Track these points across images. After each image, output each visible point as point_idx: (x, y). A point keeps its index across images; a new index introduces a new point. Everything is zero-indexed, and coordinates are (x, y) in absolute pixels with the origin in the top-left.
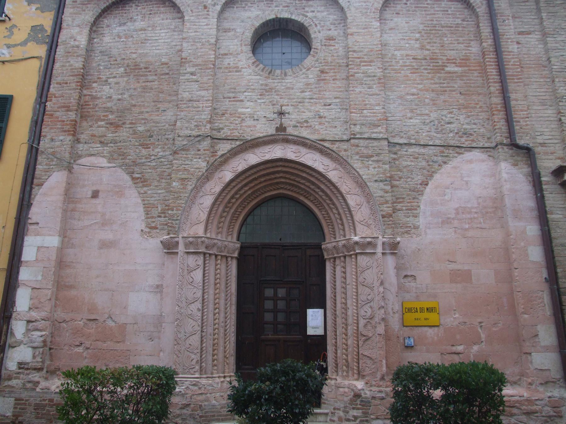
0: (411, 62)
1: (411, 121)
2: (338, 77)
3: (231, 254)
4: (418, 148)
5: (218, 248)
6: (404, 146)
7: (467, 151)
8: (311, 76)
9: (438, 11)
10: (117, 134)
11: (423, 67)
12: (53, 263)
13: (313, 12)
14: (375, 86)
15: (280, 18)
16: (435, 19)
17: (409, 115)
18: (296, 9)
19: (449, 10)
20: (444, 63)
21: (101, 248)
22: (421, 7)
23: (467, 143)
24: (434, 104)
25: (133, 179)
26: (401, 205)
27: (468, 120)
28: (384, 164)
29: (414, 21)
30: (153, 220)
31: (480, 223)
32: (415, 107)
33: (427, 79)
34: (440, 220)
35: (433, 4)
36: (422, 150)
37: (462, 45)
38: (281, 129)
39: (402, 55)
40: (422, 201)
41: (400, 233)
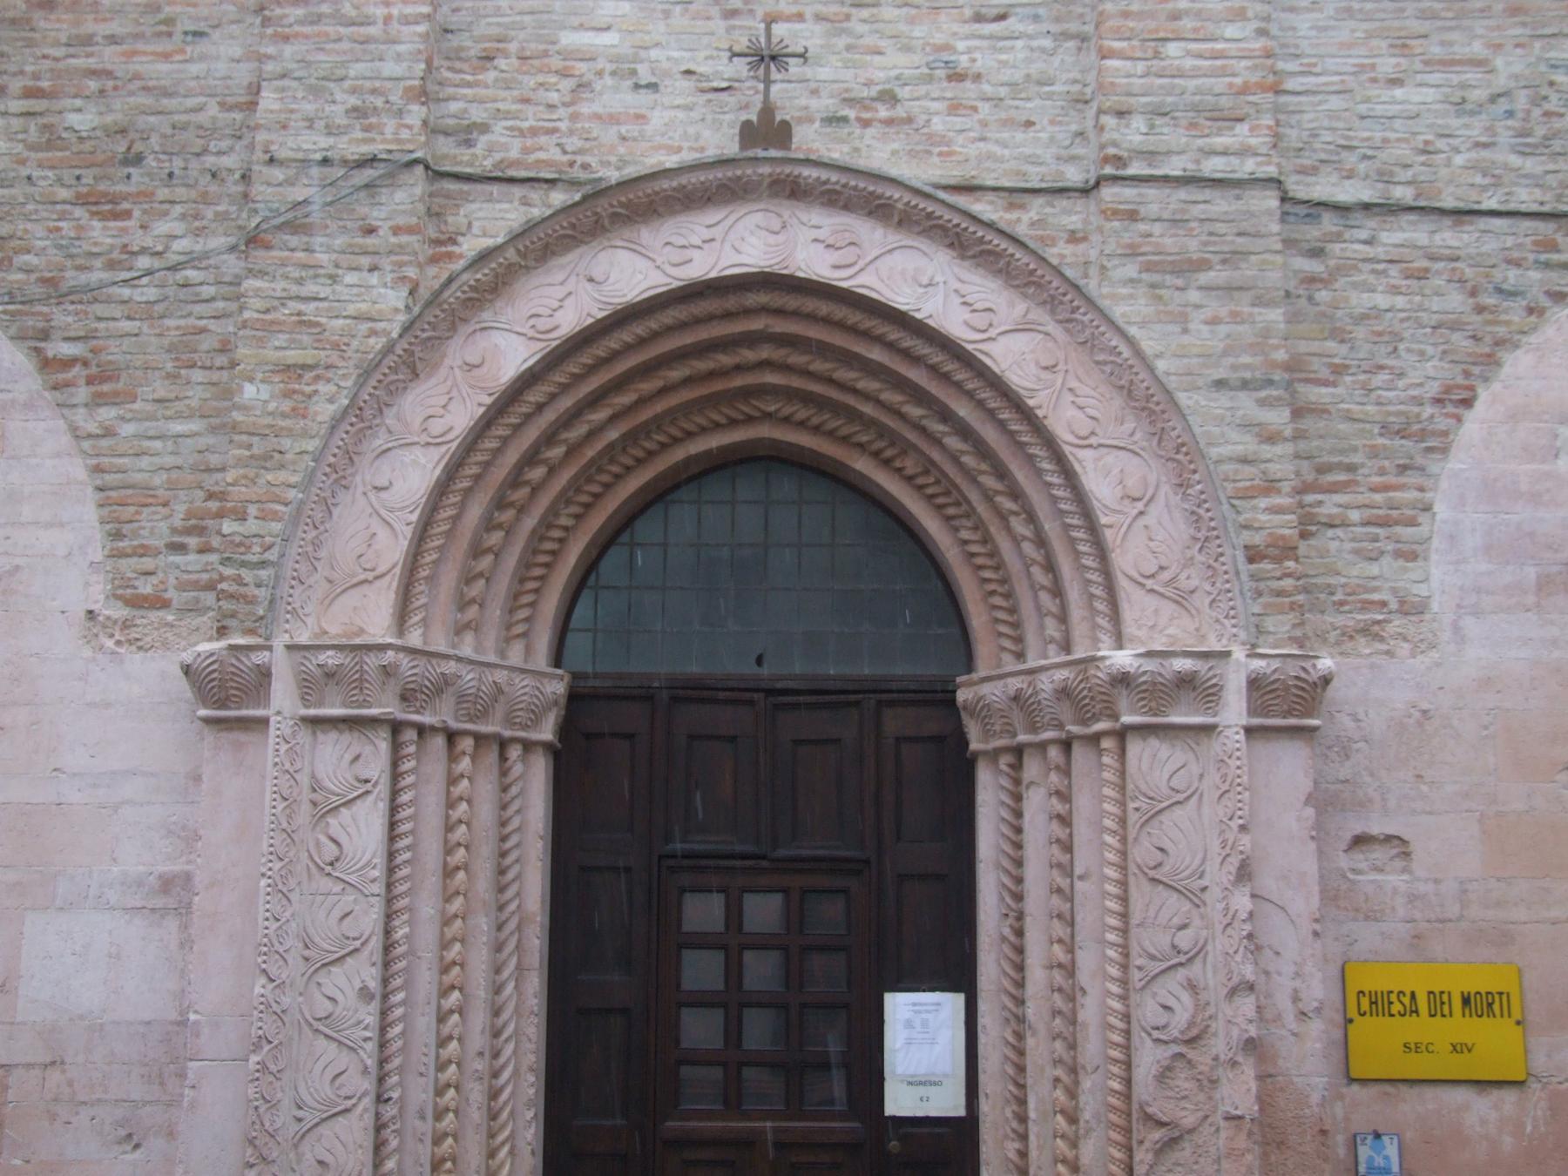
1: (1398, 93)
3: (525, 727)
6: (1357, 217)
17: (1388, 65)
25: (47, 364)
28: (1259, 302)
30: (148, 563)
32: (1417, 26)
34: (1531, 572)
36: (1448, 237)
38: (767, 131)
40: (1444, 484)
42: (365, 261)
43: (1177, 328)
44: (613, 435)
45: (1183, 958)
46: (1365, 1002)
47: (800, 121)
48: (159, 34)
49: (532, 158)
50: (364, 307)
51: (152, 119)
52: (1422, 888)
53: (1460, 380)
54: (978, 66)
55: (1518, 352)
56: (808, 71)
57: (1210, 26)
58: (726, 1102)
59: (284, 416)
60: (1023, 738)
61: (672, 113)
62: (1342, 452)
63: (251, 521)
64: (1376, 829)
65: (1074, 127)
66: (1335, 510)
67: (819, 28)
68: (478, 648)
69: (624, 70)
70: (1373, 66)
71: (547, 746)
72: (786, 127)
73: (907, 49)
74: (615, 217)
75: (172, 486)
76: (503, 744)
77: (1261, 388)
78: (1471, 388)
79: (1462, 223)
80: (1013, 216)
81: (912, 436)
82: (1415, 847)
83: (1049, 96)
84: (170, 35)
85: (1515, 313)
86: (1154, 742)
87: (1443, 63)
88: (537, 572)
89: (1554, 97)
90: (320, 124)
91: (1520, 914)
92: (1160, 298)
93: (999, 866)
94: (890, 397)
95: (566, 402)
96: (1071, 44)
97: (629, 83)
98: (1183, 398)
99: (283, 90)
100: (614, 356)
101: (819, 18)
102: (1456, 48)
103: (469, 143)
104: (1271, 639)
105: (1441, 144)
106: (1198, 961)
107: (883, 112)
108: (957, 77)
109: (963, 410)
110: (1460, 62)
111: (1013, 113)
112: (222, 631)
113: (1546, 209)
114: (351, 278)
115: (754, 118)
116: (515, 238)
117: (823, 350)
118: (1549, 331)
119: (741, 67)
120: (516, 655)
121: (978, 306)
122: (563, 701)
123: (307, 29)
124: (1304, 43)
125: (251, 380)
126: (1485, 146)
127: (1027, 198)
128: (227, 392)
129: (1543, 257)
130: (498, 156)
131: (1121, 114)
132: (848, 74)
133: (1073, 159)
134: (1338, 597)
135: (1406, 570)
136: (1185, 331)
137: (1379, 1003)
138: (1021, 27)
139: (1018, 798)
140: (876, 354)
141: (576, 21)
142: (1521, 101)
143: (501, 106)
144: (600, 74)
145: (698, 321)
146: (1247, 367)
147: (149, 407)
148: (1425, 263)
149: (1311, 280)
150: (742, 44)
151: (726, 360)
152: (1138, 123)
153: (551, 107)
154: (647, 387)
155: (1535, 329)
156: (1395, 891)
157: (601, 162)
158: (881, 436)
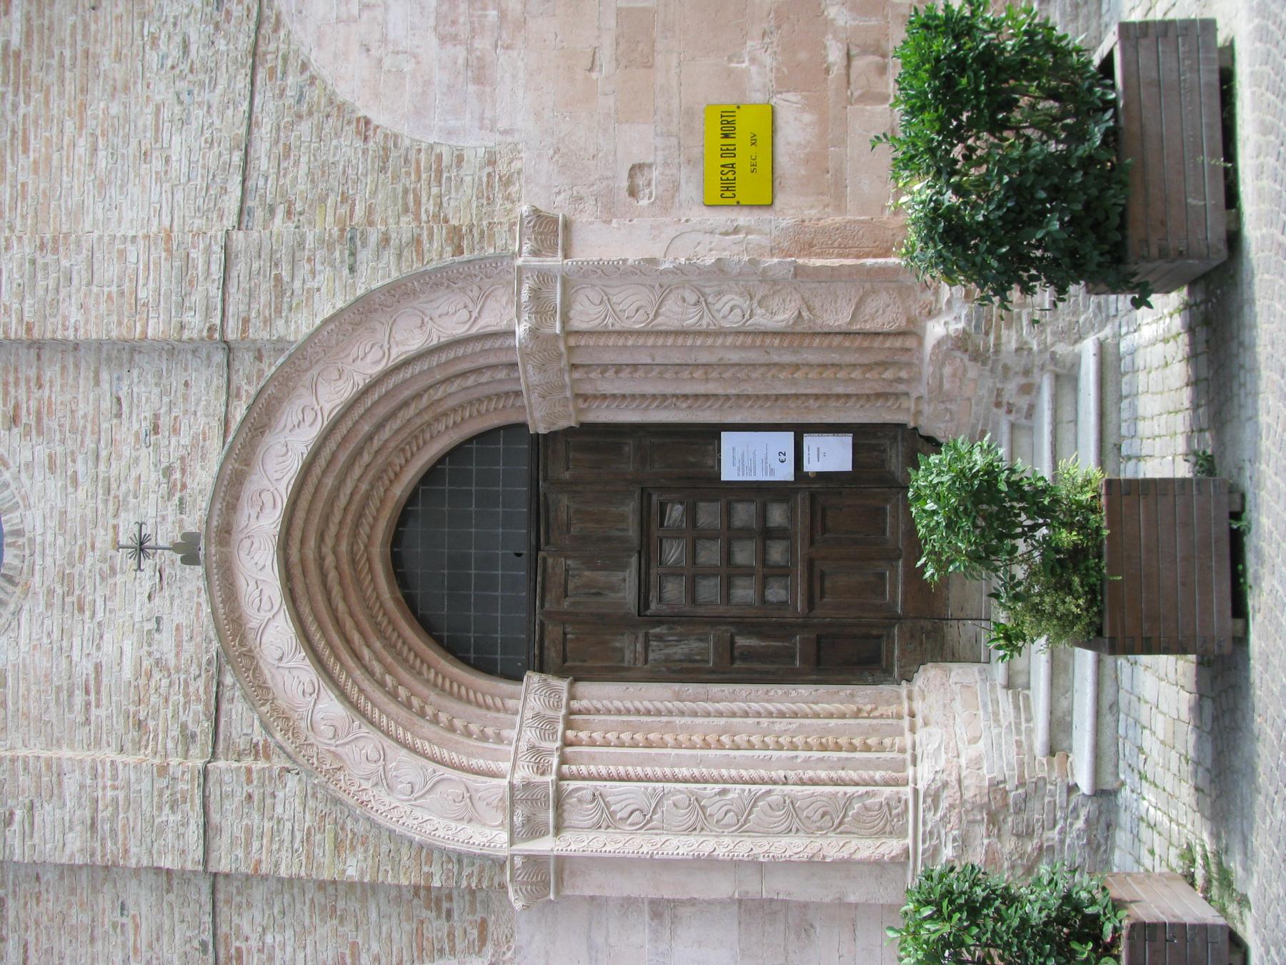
17: (157, 165)
24: (126, 89)
32: (134, 143)
34: (472, 88)
36: (264, 131)
38: (188, 551)
42: (269, 801)
44: (378, 645)
45: (702, 299)
47: (181, 527)
48: (123, 932)
49: (203, 697)
50: (297, 801)
51: (177, 936)
52: (660, 159)
54: (149, 415)
55: (338, 91)
56: (151, 522)
57: (129, 271)
58: (787, 576)
59: (366, 851)
60: (568, 394)
61: (175, 607)
62: (396, 197)
63: (432, 870)
64: (625, 184)
65: (189, 356)
66: (431, 201)
67: (123, 515)
68: (513, 726)
69: (148, 638)
70: (157, 173)
71: (571, 685)
72: (184, 536)
73: (137, 460)
74: (242, 644)
76: (571, 712)
77: (354, 244)
78: (358, 120)
79: (257, 122)
80: (244, 394)
81: (380, 459)
82: (637, 161)
83: (169, 371)
84: (123, 925)
85: (313, 94)
86: (572, 314)
87: (157, 131)
88: (463, 690)
90: (181, 830)
91: (675, 103)
92: (298, 305)
93: (646, 409)
94: (357, 471)
95: (358, 673)
96: (137, 357)
97: (157, 636)
98: (359, 292)
99: (159, 852)
100: (329, 644)
101: (116, 516)
102: (148, 123)
103: (194, 736)
104: (510, 242)
105: (207, 134)
107: (177, 475)
108: (156, 430)
109: (366, 428)
111: (179, 394)
112: (503, 886)
113: (249, 72)
114: (279, 809)
115: (179, 556)
116: (253, 707)
117: (326, 518)
119: (146, 564)
121: (300, 417)
122: (543, 676)
123: (121, 837)
124: (141, 215)
125: (344, 871)
126: (209, 107)
127: (233, 386)
128: (351, 885)
129: (279, 75)
130: (202, 717)
131: (182, 327)
132: (152, 496)
133: (209, 357)
135: (468, 161)
136: (318, 290)
137: (728, 186)
138: (125, 389)
139: (604, 397)
140: (329, 482)
141: (116, 668)
142: (182, 85)
143: (170, 716)
144: (150, 654)
146: (342, 253)
147: (361, 934)
148: (281, 145)
149: (289, 213)
150: (132, 563)
151: (332, 575)
152: (188, 317)
153: (170, 685)
154: (349, 624)
155: (324, 81)
156: (662, 174)
157: (207, 652)
158: (380, 478)
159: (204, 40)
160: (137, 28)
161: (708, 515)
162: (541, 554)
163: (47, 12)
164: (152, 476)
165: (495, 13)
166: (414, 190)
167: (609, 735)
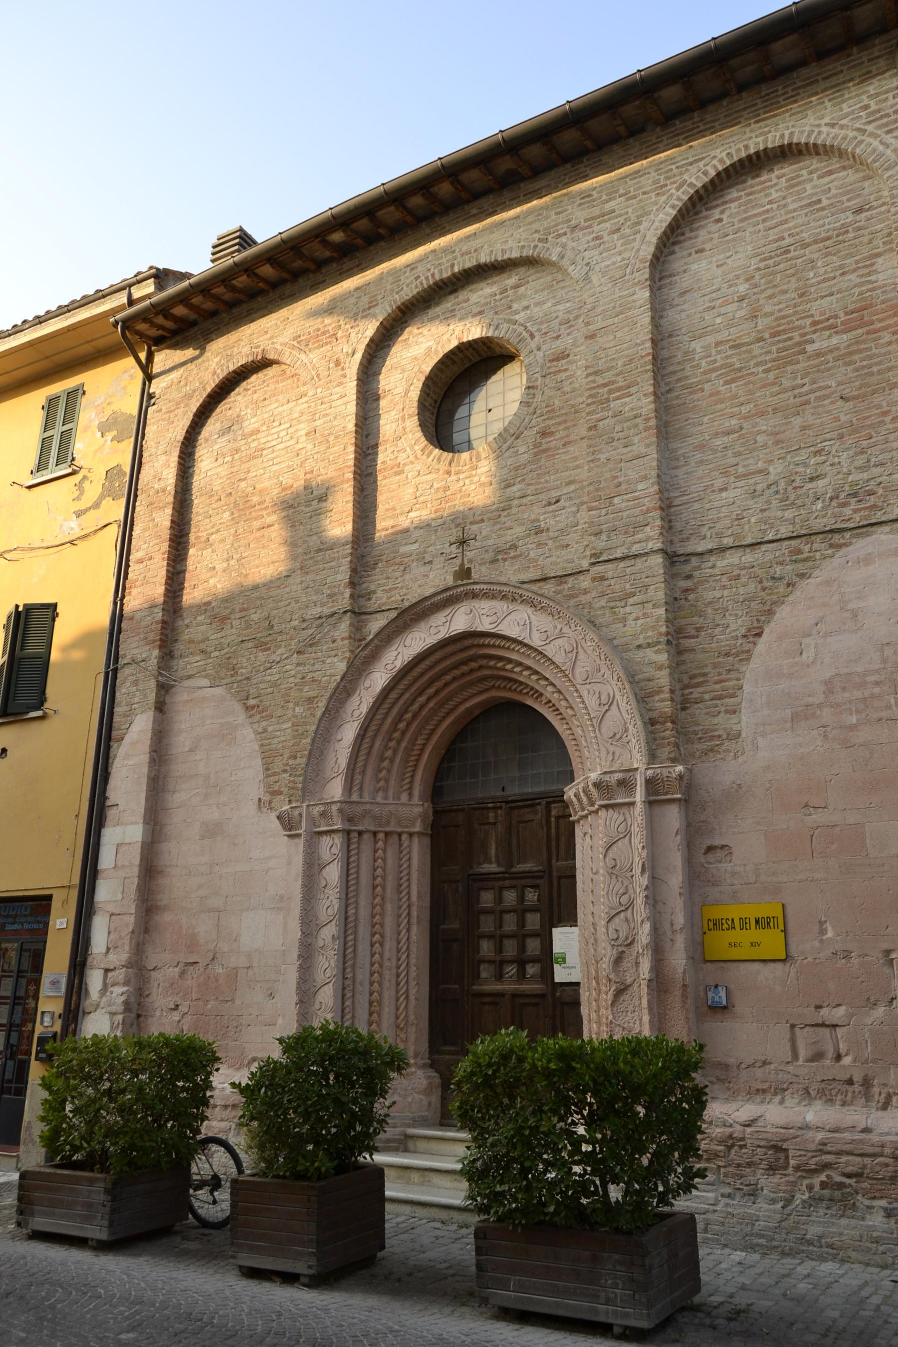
0: (727, 357)
1: (724, 494)
2: (572, 438)
3: (407, 827)
4: (740, 552)
5: (375, 818)
6: (706, 557)
7: (858, 536)
8: (522, 449)
9: (795, 210)
10: (222, 634)
11: (752, 363)
12: (136, 871)
13: (527, 308)
14: (636, 440)
15: (469, 342)
16: (786, 235)
17: (718, 483)
18: (496, 313)
19: (823, 198)
20: (805, 334)
21: (203, 838)
22: (756, 215)
23: (857, 517)
24: (777, 443)
25: (247, 708)
26: (700, 689)
27: (860, 460)
28: (654, 606)
29: (739, 256)
30: (276, 778)
31: (889, 707)
32: (732, 461)
33: (764, 386)
34: (789, 712)
35: (784, 198)
36: (749, 557)
37: (853, 277)
38: (464, 573)
39: (706, 348)
40: (748, 675)
41: (697, 754)
43: (621, 625)
46: (711, 924)
52: (737, 869)
53: (755, 624)
68: (386, 798)
74: (411, 619)
75: (284, 748)
78: (761, 627)
87: (744, 476)
89: (798, 479)
100: (422, 675)
106: (630, 910)
110: (753, 473)
118: (798, 593)
120: (404, 797)
127: (567, 578)
134: (700, 735)
145: (453, 654)
150: (453, 540)
151: (465, 668)
152: (604, 537)
154: (439, 684)
159: (821, 491)
160: (828, 436)
161: (533, 921)
162: (503, 805)
163: (840, 362)
164: (510, 536)
165: (854, 721)
166: (707, 681)
167: (380, 861)
